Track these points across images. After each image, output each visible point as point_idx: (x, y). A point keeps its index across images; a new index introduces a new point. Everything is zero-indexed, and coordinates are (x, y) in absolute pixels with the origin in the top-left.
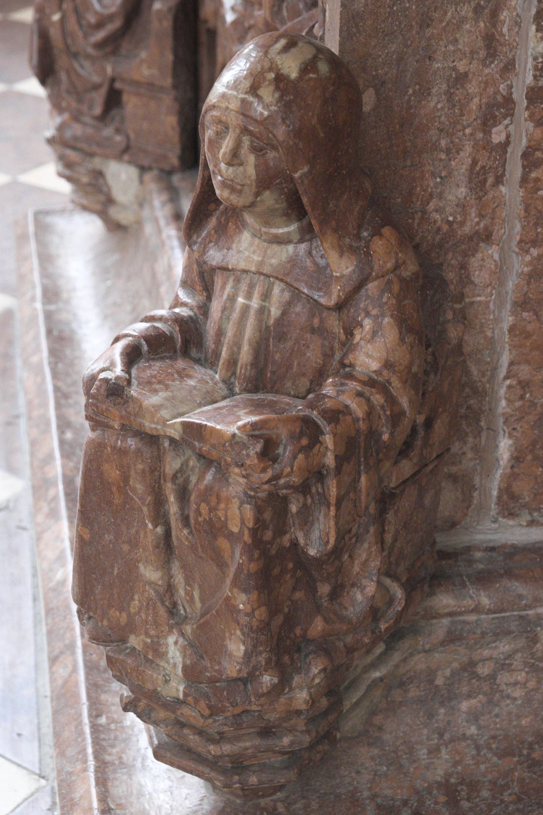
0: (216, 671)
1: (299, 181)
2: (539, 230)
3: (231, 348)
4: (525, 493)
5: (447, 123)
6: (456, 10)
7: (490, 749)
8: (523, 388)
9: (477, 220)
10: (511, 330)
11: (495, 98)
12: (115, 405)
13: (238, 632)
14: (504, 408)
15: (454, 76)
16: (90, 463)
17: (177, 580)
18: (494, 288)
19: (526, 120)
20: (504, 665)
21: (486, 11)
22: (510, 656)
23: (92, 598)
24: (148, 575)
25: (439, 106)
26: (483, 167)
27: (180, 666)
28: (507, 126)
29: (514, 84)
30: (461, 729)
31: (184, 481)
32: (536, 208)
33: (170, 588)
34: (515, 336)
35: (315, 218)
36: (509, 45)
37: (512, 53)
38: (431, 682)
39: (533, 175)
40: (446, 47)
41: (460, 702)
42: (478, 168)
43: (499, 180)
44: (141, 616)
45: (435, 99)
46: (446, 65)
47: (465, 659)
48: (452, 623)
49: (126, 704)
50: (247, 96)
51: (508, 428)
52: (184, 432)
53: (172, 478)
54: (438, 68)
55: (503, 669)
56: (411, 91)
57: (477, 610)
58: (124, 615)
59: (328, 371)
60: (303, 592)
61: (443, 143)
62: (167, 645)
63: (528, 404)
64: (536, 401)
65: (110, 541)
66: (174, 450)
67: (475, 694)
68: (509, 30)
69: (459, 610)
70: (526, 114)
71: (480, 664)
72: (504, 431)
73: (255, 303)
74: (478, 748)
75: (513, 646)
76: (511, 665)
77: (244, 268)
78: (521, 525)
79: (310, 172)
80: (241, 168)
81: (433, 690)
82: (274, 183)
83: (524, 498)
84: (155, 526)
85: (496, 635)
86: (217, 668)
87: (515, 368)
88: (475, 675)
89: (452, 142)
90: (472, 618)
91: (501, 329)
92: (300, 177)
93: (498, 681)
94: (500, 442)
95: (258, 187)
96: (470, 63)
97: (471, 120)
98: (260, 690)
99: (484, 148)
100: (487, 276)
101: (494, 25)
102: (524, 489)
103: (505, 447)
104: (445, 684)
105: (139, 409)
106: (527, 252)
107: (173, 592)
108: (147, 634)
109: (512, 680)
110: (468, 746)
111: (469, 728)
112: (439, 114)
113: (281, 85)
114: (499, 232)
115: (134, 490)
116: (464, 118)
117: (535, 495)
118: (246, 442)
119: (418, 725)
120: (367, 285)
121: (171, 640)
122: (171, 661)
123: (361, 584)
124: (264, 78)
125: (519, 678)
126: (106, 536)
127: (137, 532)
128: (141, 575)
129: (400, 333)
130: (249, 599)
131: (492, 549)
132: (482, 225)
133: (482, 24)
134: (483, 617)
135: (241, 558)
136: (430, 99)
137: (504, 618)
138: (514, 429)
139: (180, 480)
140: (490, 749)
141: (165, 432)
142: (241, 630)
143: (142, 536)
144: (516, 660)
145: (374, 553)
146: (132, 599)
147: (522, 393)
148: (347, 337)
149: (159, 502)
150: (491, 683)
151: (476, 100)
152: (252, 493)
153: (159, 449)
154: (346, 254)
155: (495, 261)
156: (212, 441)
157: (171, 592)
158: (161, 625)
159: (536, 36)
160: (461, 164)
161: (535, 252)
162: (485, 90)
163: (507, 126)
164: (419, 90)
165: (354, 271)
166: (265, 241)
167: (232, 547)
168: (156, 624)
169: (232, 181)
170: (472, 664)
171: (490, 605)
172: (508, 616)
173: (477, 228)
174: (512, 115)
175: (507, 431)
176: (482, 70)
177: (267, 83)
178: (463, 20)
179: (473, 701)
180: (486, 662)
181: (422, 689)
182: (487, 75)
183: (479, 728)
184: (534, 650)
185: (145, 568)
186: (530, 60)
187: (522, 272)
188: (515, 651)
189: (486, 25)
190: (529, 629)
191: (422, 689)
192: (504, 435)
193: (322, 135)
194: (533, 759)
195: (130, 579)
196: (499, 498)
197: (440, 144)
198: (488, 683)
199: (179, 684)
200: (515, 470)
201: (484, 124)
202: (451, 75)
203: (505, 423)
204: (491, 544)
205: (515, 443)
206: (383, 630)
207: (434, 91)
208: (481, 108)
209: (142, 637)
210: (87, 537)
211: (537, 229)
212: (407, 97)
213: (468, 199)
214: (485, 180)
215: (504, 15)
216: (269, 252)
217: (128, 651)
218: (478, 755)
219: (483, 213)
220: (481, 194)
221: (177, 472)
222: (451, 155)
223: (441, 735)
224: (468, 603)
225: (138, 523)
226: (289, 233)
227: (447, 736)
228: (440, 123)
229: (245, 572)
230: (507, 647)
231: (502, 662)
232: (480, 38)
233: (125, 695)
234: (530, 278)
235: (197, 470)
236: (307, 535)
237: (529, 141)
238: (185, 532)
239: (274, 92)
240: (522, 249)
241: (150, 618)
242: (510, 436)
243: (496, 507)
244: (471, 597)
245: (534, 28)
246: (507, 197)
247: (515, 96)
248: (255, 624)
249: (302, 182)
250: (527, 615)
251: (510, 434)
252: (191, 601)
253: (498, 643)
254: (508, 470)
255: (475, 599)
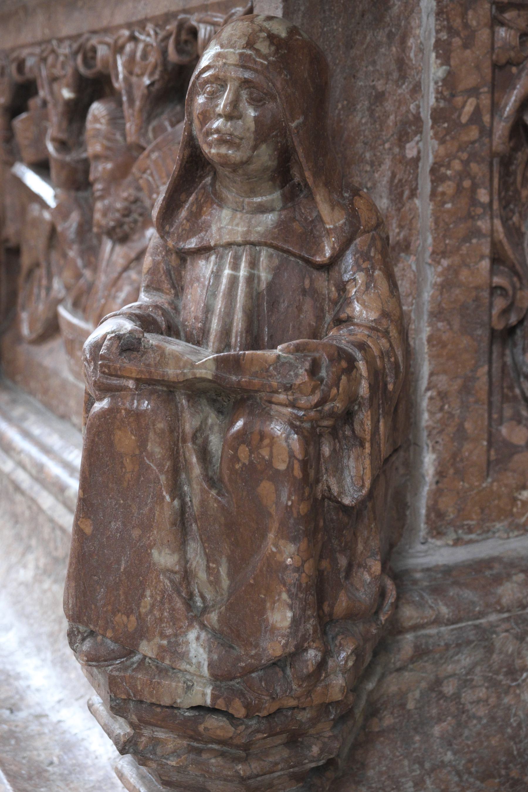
0: (252, 657)
1: (296, 131)
2: (447, 242)
3: (223, 319)
4: (450, 510)
5: (370, 137)
6: (374, 35)
7: (470, 773)
8: (442, 399)
9: (397, 230)
10: (430, 340)
11: (407, 116)
12: (130, 360)
13: (285, 596)
14: (427, 421)
15: (374, 94)
16: (98, 435)
17: (194, 564)
18: (414, 298)
19: (432, 138)
20: (466, 682)
21: (397, 37)
22: (470, 671)
23: (93, 607)
24: (162, 561)
25: (364, 121)
26: (400, 180)
27: (206, 664)
28: (417, 143)
29: (421, 104)
30: (439, 756)
31: (203, 442)
32: (444, 220)
33: (187, 575)
34: (433, 346)
35: (309, 169)
36: (416, 68)
37: (419, 76)
38: (403, 706)
39: (440, 189)
40: (366, 67)
41: (432, 727)
42: (396, 181)
43: (413, 194)
44: (154, 615)
45: (360, 115)
46: (367, 84)
47: (432, 677)
48: (417, 637)
49: (125, 744)
50: (244, 51)
51: (431, 441)
52: (217, 369)
53: (193, 438)
54: (361, 86)
55: (465, 687)
56: (340, 106)
57: (437, 621)
58: (133, 618)
59: (321, 334)
60: (328, 560)
61: (368, 155)
62: (188, 643)
63: (447, 416)
64: (454, 412)
65: (117, 529)
66: (192, 406)
67: (444, 717)
68: (416, 56)
69: (422, 621)
70: (431, 133)
71: (445, 682)
72: (428, 445)
73: (243, 272)
74: (459, 774)
75: (473, 658)
76: (472, 680)
77: (229, 240)
78: (448, 545)
79: (304, 123)
80: (240, 122)
81: (406, 716)
82: (271, 135)
83: (449, 516)
84: (173, 499)
85: (458, 645)
86: (253, 652)
87: (434, 378)
88: (441, 695)
89: (375, 155)
90: (432, 631)
91: (421, 339)
92: (296, 127)
93: (463, 700)
94: (424, 457)
95: (256, 139)
96: (386, 84)
97: (389, 135)
98: (305, 671)
99: (400, 162)
100: (408, 286)
101: (404, 51)
102: (448, 505)
103: (429, 461)
104: (416, 708)
105: (161, 356)
106: (439, 263)
107: (190, 579)
108: (162, 635)
109: (475, 698)
110: (449, 772)
111: (446, 754)
112: (363, 128)
113: (275, 41)
114: (416, 243)
115: (151, 456)
116: (384, 133)
117: (459, 511)
118: (292, 361)
119: (398, 757)
120: (355, 239)
121: (192, 635)
122: (194, 661)
123: (366, 565)
124: (258, 37)
125: (481, 695)
126: (113, 524)
127: (151, 510)
128: (154, 564)
129: (389, 286)
130: (298, 550)
131: (428, 570)
132: (402, 235)
133: (394, 49)
134: (443, 629)
135: (289, 499)
136: (355, 114)
137: (461, 628)
138: (437, 442)
139: (200, 441)
140: (470, 773)
141: (194, 374)
142: (288, 591)
143: (157, 513)
144: (476, 675)
145: (374, 530)
146: (143, 596)
147: (441, 404)
148: (339, 294)
149: (177, 470)
150: (456, 703)
151: (392, 117)
152: (298, 423)
153: (177, 407)
154: (336, 208)
155: (413, 271)
156: (253, 370)
157: (187, 579)
158: (179, 619)
159: (436, 62)
160: (383, 176)
161: (445, 263)
162: (398, 108)
163: (417, 143)
164: (347, 105)
165: (345, 224)
166: (247, 213)
167: (277, 490)
168: (174, 620)
169: (231, 135)
170: (438, 682)
171: (448, 614)
172: (464, 627)
173: (398, 238)
174: (421, 133)
175: (430, 445)
176: (396, 90)
177: (261, 40)
178: (379, 44)
180: (451, 679)
181: (396, 715)
182: (399, 95)
183: (455, 753)
184: (491, 662)
185: (160, 553)
186: (432, 84)
187: (436, 282)
188: (475, 664)
189: (397, 50)
190: (486, 637)
191: (396, 715)
192: (428, 449)
193: (312, 89)
194: (513, 778)
195: (140, 571)
196: (428, 516)
197: (365, 156)
198: (454, 702)
199: (205, 687)
200: (440, 485)
201: (400, 140)
202: (372, 93)
203: (429, 435)
204: (425, 566)
205: (438, 457)
206: (383, 622)
207: (359, 107)
208: (396, 125)
209: (157, 640)
210: (88, 530)
211: (445, 240)
212: (337, 112)
213: (390, 210)
214: (402, 194)
215: (411, 42)
216: (253, 221)
217: (135, 666)
218: (461, 781)
219: (402, 224)
220: (400, 205)
221: (196, 432)
222: (374, 168)
223: (421, 764)
225: (152, 498)
226: (273, 200)
227: (427, 765)
228: (365, 136)
229: (295, 515)
230: (468, 659)
231: (464, 678)
232: (393, 62)
233: (122, 734)
234: (442, 288)
235: (216, 428)
236: (340, 482)
237: (435, 157)
238: (213, 492)
239: (269, 46)
240: (434, 260)
241: (166, 614)
242: (434, 450)
243: (426, 526)
244: (431, 607)
245: (434, 55)
246: (420, 210)
247: (422, 115)
248: (304, 580)
249: (298, 132)
250: (481, 624)
251: (433, 447)
252: (215, 582)
253: (460, 655)
254: (434, 487)
255: (435, 608)
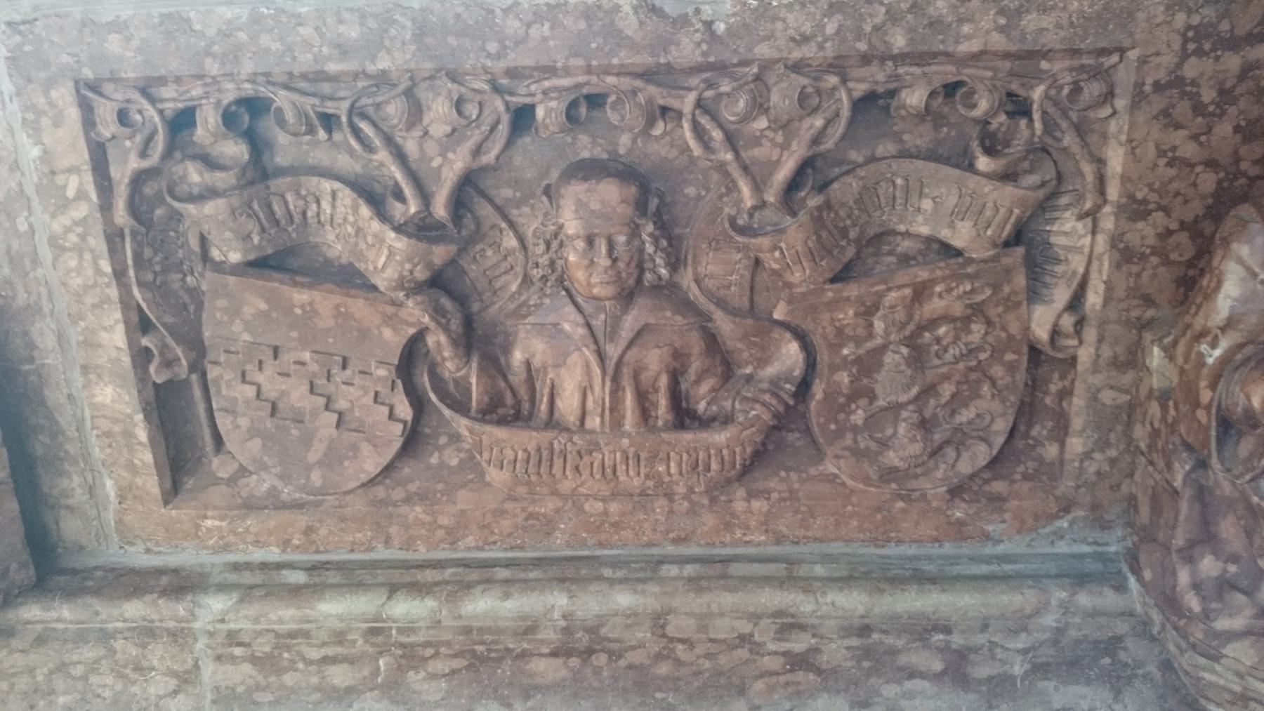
22: (96, 661)
88: (69, 675)
179: (69, 697)
224: (54, 615)
